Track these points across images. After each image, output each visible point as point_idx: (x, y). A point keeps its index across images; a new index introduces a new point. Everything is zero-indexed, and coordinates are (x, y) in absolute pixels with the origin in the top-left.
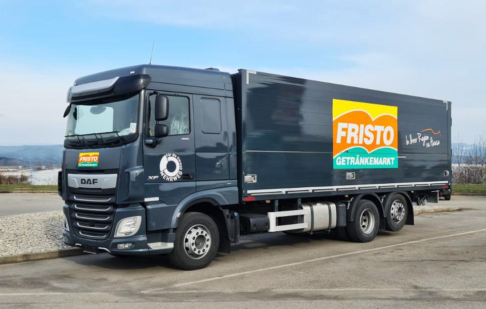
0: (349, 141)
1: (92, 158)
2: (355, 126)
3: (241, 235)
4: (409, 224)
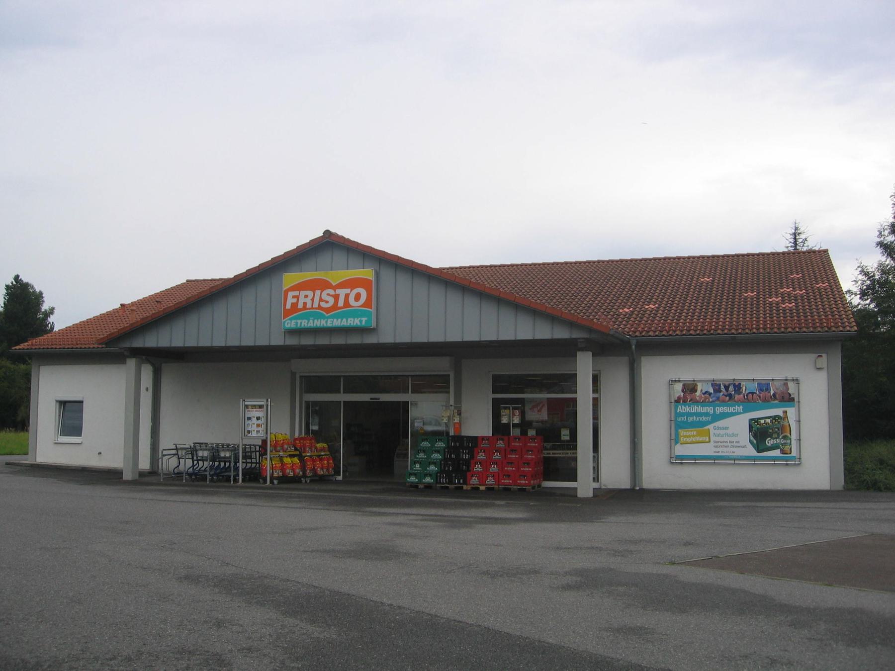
0: (300, 306)
1: (342, 292)
2: (310, 293)
3: (575, 479)
4: (331, 393)
